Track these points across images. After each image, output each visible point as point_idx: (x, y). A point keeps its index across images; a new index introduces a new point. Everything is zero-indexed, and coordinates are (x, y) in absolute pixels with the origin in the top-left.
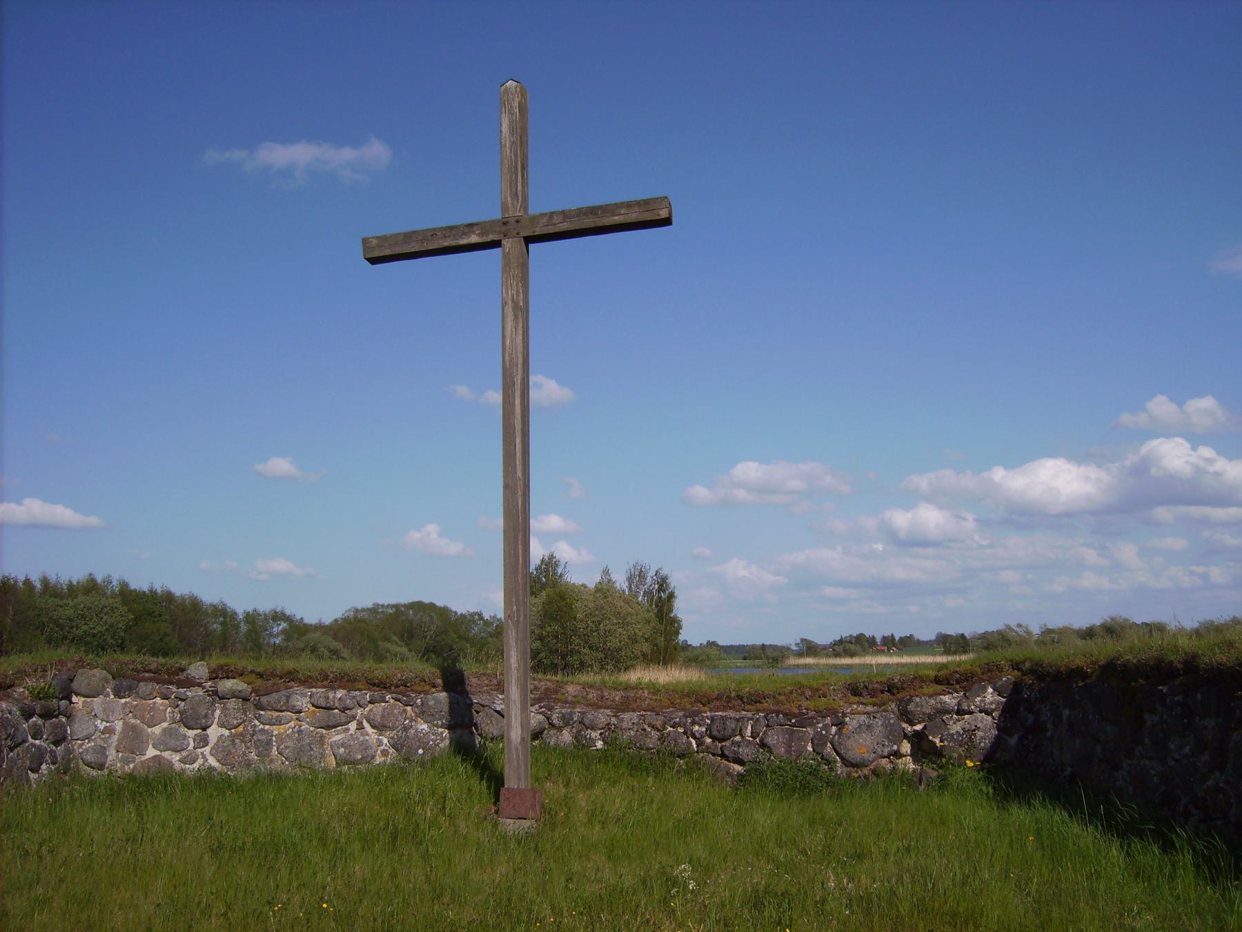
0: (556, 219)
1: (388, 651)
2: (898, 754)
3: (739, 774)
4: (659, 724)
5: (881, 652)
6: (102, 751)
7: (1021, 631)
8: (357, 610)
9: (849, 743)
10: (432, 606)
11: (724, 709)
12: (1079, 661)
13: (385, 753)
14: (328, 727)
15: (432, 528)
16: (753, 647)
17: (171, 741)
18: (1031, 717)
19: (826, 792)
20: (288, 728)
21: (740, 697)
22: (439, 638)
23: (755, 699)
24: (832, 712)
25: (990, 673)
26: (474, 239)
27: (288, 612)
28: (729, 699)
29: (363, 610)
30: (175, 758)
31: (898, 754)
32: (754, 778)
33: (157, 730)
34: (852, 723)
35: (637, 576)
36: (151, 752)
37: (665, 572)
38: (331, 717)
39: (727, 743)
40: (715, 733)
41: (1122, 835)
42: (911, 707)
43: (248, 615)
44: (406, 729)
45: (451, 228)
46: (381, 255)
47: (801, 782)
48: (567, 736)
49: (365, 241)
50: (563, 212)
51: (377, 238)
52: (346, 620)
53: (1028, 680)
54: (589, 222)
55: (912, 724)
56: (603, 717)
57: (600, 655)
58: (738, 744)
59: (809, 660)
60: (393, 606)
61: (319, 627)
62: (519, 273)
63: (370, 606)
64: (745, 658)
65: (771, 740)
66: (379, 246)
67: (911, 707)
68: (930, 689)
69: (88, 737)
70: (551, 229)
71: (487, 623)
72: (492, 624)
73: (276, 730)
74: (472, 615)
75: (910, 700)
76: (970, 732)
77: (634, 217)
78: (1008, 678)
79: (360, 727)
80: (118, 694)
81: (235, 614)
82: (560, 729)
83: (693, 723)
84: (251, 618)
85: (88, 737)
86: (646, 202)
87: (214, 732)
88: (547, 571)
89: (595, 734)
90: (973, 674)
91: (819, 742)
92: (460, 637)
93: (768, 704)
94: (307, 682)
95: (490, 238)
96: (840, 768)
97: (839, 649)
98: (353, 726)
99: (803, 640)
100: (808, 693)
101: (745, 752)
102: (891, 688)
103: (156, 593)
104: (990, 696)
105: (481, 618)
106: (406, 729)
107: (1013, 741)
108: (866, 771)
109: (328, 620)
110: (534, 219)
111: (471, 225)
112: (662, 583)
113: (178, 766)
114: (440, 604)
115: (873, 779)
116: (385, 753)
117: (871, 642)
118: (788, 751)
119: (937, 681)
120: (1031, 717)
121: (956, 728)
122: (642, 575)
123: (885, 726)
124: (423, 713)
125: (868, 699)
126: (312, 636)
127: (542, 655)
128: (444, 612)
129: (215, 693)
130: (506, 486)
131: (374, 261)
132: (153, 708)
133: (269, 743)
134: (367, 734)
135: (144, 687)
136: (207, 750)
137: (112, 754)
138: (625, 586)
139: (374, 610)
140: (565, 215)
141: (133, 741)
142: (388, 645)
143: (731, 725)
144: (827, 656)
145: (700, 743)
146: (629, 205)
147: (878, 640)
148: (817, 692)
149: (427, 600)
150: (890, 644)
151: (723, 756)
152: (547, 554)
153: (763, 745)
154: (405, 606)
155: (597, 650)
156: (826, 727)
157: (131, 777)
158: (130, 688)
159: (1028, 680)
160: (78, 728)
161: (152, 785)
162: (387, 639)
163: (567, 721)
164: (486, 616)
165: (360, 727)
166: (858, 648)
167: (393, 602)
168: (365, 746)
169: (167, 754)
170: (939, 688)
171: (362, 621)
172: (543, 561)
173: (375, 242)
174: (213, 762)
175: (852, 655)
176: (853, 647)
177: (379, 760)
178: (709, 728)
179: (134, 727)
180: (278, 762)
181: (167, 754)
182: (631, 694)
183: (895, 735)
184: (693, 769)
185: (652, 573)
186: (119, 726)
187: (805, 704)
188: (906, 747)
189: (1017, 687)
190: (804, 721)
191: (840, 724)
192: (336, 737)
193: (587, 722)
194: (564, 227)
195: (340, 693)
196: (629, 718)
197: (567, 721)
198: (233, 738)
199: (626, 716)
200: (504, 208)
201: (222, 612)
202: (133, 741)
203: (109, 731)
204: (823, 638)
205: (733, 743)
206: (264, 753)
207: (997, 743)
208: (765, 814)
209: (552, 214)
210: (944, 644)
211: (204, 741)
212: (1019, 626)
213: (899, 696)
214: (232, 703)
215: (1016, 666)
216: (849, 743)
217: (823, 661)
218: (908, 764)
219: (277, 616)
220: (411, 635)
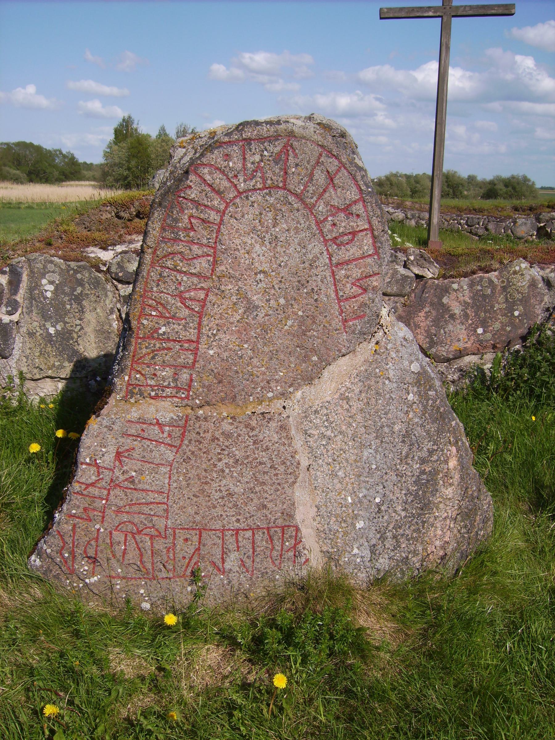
0: (467, 9)
1: (8, 173)
4: (448, 219)
9: (518, 230)
10: (31, 145)
11: (469, 214)
15: (31, 89)
21: (475, 210)
22: (37, 166)
24: (509, 217)
26: (431, 14)
28: (470, 211)
34: (519, 222)
39: (473, 228)
40: (469, 223)
42: (541, 217)
45: (421, 8)
48: (413, 223)
49: (381, 9)
50: (470, 6)
51: (387, 8)
54: (481, 12)
58: (478, 228)
60: (6, 144)
62: (445, 30)
66: (387, 12)
67: (541, 217)
68: (547, 210)
70: (465, 13)
71: (64, 156)
74: (56, 151)
75: (540, 214)
77: (500, 11)
82: (411, 219)
83: (461, 219)
86: (506, 5)
88: (127, 126)
89: (423, 222)
92: (50, 165)
95: (438, 14)
100: (500, 209)
102: (531, 209)
110: (457, 8)
111: (429, 7)
114: (36, 143)
119: (548, 207)
125: (521, 212)
127: (130, 178)
128: (38, 149)
131: (381, 18)
140: (471, 7)
146: (499, 6)
149: (28, 141)
152: (126, 116)
153: (487, 229)
156: (510, 223)
163: (413, 216)
164: (64, 152)
170: (550, 210)
172: (124, 120)
173: (386, 10)
191: (515, 222)
193: (421, 217)
194: (471, 12)
197: (413, 216)
205: (476, 228)
209: (466, 6)
213: (535, 212)
216: (518, 230)
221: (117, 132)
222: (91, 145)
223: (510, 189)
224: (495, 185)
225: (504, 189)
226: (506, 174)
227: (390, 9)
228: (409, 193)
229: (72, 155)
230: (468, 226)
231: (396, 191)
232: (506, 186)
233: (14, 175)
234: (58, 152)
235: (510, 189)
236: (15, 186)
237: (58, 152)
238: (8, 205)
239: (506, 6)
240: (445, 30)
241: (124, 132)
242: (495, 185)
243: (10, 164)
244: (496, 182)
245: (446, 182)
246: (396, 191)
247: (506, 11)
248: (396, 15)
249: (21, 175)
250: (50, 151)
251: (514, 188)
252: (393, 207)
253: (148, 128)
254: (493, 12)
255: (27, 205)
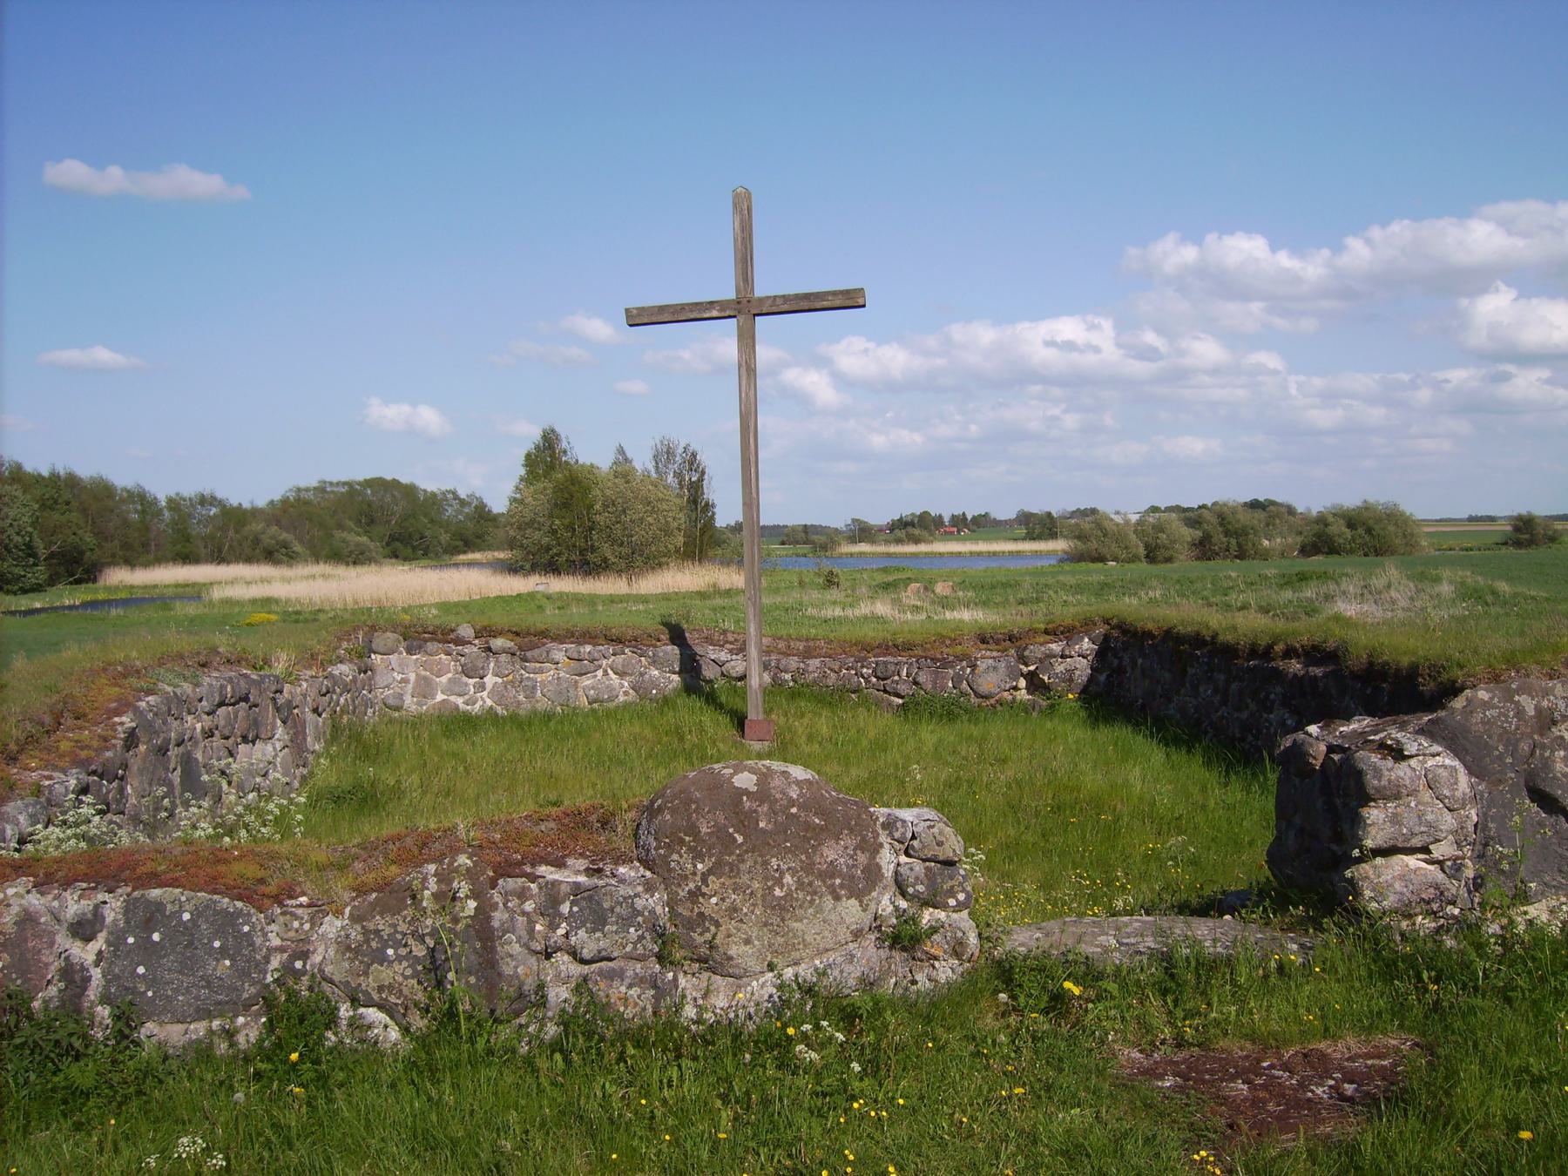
0: (779, 301)
2: (1016, 688)
3: (898, 706)
5: (948, 536)
6: (400, 696)
7: (1118, 519)
8: (299, 490)
12: (1150, 626)
13: (626, 693)
14: (581, 675)
16: (794, 529)
17: (454, 688)
18: (1116, 662)
19: (965, 718)
20: (549, 675)
23: (907, 647)
25: (1086, 625)
26: (715, 313)
27: (219, 495)
28: (887, 648)
29: (307, 490)
30: (460, 701)
31: (1016, 688)
32: (911, 709)
33: (444, 679)
34: (982, 665)
35: (665, 454)
36: (440, 697)
37: (694, 447)
38: (582, 667)
41: (1167, 745)
42: (1026, 653)
43: (170, 501)
44: (642, 675)
46: (639, 318)
47: (948, 712)
49: (627, 310)
52: (285, 501)
53: (1115, 633)
54: (805, 305)
55: (1027, 665)
56: (793, 662)
57: (625, 550)
59: (864, 547)
60: (345, 484)
61: (255, 513)
62: (747, 340)
63: (315, 484)
64: (783, 543)
65: (921, 679)
67: (1026, 653)
69: (387, 686)
70: (774, 309)
71: (463, 503)
72: (469, 504)
73: (539, 678)
75: (1025, 649)
76: (1070, 672)
77: (838, 303)
78: (1100, 630)
79: (606, 673)
80: (410, 652)
81: (155, 501)
84: (174, 504)
85: (387, 686)
86: (848, 292)
87: (490, 680)
90: (1074, 628)
91: (957, 680)
92: (432, 521)
93: (918, 651)
94: (560, 639)
96: (973, 699)
97: (900, 534)
98: (600, 673)
99: (854, 521)
101: (903, 688)
103: (59, 477)
104: (1086, 645)
105: (456, 497)
106: (642, 675)
107: (1102, 678)
108: (992, 701)
109: (261, 503)
110: (761, 300)
111: (712, 303)
112: (692, 461)
113: (462, 707)
115: (999, 708)
116: (626, 693)
117: (938, 521)
118: (934, 687)
119: (1046, 632)
120: (1116, 662)
121: (1060, 668)
122: (670, 452)
123: (1007, 667)
124: (654, 662)
125: (993, 646)
126: (257, 527)
128: (410, 491)
129: (489, 649)
130: (744, 504)
132: (440, 662)
133: (534, 687)
134: (611, 679)
135: (430, 646)
136: (485, 694)
137: (408, 701)
138: (651, 466)
139: (321, 489)
140: (785, 298)
141: (425, 689)
142: (345, 535)
143: (892, 668)
144: (887, 542)
145: (867, 681)
146: (834, 293)
147: (946, 519)
148: (955, 641)
150: (964, 525)
151: (885, 691)
153: (916, 683)
154: (359, 483)
155: (621, 545)
156: (963, 669)
157: (420, 716)
158: (420, 647)
159: (1115, 633)
160: (381, 680)
161: (459, 724)
162: (341, 526)
164: (463, 496)
165: (606, 673)
166: (925, 533)
167: (344, 479)
168: (610, 688)
169: (452, 698)
171: (307, 503)
174: (489, 702)
175: (917, 541)
176: (917, 532)
177: (622, 698)
178: (874, 671)
179: (425, 678)
180: (543, 704)
181: (452, 698)
182: (811, 644)
183: (1014, 674)
184: (865, 702)
185: (681, 450)
186: (412, 677)
187: (946, 650)
188: (1022, 683)
189: (1106, 637)
190: (946, 664)
191: (974, 667)
192: (587, 681)
194: (785, 307)
195: (588, 648)
196: (814, 663)
198: (505, 685)
199: (810, 662)
200: (738, 291)
201: (141, 498)
202: (425, 689)
203: (405, 681)
204: (880, 516)
206: (530, 695)
207: (1091, 679)
208: (930, 734)
210: (1027, 524)
211: (483, 687)
212: (1117, 513)
214: (503, 657)
215: (1107, 622)
217: (881, 549)
218: (1023, 695)
219: (205, 501)
220: (372, 521)
221: (531, 461)
222: (494, 482)
223: (1361, 531)
224: (1326, 525)
225: (1348, 533)
226: (1350, 499)
227: (642, 310)
228: (1142, 551)
229: (480, 500)
230: (878, 678)
231: (1114, 548)
232: (1351, 525)
233: (358, 545)
234: (450, 496)
235: (1361, 531)
236: (341, 570)
237: (450, 496)
238: (294, 617)
239: (846, 293)
240: (747, 340)
241: (546, 458)
242: (1326, 525)
243: (351, 524)
244: (1331, 519)
245: (1221, 525)
246: (1114, 548)
247: (850, 300)
248: (654, 319)
249: (372, 545)
250: (434, 495)
251: (1369, 531)
252: (731, 651)
253: (590, 451)
254: (825, 304)
255: (331, 614)
